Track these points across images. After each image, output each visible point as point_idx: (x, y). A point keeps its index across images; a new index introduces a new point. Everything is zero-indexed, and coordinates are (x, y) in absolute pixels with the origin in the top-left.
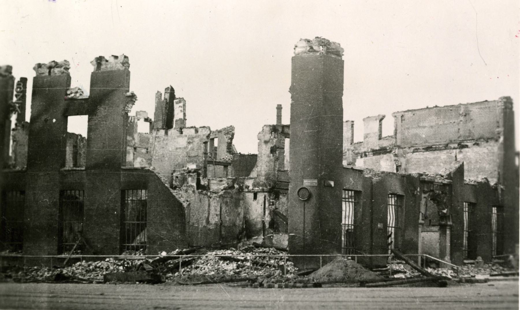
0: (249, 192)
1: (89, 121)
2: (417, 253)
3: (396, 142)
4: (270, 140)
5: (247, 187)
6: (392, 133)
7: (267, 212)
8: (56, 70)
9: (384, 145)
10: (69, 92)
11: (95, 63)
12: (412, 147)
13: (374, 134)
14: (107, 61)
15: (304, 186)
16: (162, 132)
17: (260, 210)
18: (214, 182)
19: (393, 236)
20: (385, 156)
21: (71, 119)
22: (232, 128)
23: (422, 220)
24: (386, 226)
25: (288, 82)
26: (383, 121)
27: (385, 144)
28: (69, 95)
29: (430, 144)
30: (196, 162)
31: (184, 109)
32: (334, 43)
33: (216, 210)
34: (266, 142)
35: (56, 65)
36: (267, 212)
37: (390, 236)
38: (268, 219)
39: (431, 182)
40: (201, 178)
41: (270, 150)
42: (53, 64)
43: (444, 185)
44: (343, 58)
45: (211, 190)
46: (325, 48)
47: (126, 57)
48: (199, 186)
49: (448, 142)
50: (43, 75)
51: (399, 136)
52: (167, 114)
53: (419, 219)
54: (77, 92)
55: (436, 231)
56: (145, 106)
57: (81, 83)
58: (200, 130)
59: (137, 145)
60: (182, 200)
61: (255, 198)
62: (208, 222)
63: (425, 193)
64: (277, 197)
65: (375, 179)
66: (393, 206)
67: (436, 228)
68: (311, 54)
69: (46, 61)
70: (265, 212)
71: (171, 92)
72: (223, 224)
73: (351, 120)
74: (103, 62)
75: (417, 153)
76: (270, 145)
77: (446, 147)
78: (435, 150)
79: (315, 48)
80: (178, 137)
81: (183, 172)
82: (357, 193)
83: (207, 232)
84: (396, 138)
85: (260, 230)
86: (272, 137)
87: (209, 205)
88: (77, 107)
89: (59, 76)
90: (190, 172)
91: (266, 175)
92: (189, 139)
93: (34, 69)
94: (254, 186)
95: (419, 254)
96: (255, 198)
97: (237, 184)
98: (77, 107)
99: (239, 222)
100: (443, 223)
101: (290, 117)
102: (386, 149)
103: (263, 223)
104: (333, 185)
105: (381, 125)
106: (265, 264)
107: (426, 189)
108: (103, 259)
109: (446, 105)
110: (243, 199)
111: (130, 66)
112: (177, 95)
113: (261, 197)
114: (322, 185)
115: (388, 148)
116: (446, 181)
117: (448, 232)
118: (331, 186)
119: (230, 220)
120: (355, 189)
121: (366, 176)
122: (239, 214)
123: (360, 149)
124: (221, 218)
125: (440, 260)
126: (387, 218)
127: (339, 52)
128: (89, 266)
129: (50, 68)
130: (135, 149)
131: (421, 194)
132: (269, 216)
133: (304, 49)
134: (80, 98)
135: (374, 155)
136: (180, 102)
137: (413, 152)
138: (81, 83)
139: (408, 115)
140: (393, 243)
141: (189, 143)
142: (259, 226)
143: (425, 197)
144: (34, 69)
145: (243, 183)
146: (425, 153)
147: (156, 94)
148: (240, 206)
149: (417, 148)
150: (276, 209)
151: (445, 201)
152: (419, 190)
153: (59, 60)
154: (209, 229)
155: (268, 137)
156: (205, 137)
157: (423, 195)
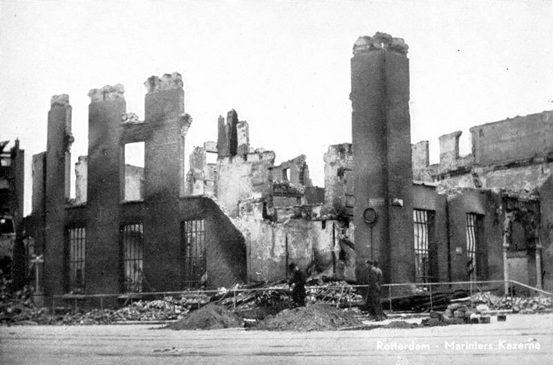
0: (318, 220)
1: (146, 147)
2: (503, 278)
3: (475, 161)
4: (336, 160)
5: (315, 215)
6: (469, 151)
7: (337, 242)
8: (111, 95)
9: (463, 165)
10: (124, 118)
11: (148, 83)
12: (493, 164)
13: (450, 152)
14: (160, 81)
15: (370, 206)
16: (227, 159)
17: (330, 240)
18: (281, 211)
19: (474, 263)
20: (464, 178)
21: (129, 147)
22: (303, 157)
23: (507, 242)
24: (465, 250)
25: (349, 90)
26: (461, 138)
27: (463, 163)
28: (125, 121)
29: (512, 160)
30: (262, 191)
31: (247, 133)
32: (397, 39)
33: (281, 241)
34: (332, 164)
35: (113, 90)
36: (337, 242)
37: (471, 262)
38: (337, 249)
39: (514, 199)
40: (267, 208)
41: (337, 171)
42: (108, 89)
43: (533, 201)
44: (408, 56)
45: (278, 220)
46: (387, 45)
47: (178, 74)
48: (265, 216)
49: (533, 155)
50: (99, 101)
51: (478, 154)
52: (231, 140)
53: (503, 242)
54: (132, 117)
55: (523, 257)
56: (202, 133)
57: (136, 109)
58: (264, 155)
59: (206, 178)
60: (241, 230)
61: (324, 227)
62: (272, 254)
63: (509, 211)
64: (347, 225)
65: (451, 197)
66: (473, 228)
67: (523, 253)
68: (371, 53)
69: (100, 86)
70: (334, 242)
71: (234, 116)
72: (290, 257)
73: (425, 140)
74: (157, 83)
75: (499, 171)
76: (337, 167)
77: (531, 162)
78: (517, 167)
79: (376, 45)
80: (243, 163)
81: (249, 202)
82: (431, 213)
83: (273, 265)
84: (474, 156)
85: (330, 262)
86: (338, 158)
87: (274, 236)
88: (134, 132)
89: (115, 101)
90: (255, 202)
91: (334, 201)
92: (253, 165)
93: (89, 95)
94: (322, 213)
95: (506, 280)
96: (324, 227)
97: (305, 212)
98: (134, 132)
99: (308, 255)
100: (531, 246)
101: (351, 128)
102: (465, 169)
103: (333, 253)
104: (402, 204)
105: (457, 143)
106: (330, 298)
107: (509, 207)
108: (161, 297)
109: (489, 122)
110: (311, 228)
111: (184, 84)
112: (240, 119)
113: (329, 225)
114: (388, 205)
115: (466, 168)
116: (533, 197)
117: (538, 257)
118: (399, 205)
119: (297, 251)
120: (428, 208)
121: (439, 193)
122: (307, 245)
123: (437, 171)
124: (287, 250)
125: (530, 287)
126: (466, 241)
127: (403, 48)
128: (144, 306)
129: (105, 92)
130: (205, 182)
131: (504, 213)
132: (339, 246)
133: (363, 48)
134: (136, 122)
135: (452, 176)
136: (243, 125)
137: (494, 170)
138: (136, 109)
139: (486, 130)
140: (475, 270)
141: (253, 170)
142: (329, 258)
143: (509, 217)
144: (89, 95)
145: (310, 211)
146: (507, 170)
147: (219, 119)
148: (308, 236)
149: (498, 165)
150: (347, 237)
151: (532, 220)
152: (501, 208)
153: (113, 84)
154: (275, 262)
155: (333, 158)
156: (269, 163)
157: (506, 215)
